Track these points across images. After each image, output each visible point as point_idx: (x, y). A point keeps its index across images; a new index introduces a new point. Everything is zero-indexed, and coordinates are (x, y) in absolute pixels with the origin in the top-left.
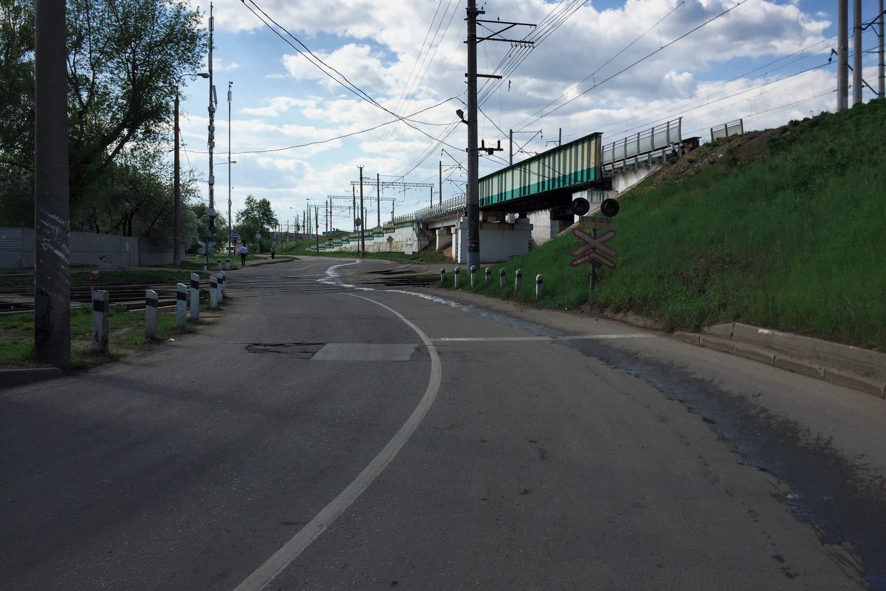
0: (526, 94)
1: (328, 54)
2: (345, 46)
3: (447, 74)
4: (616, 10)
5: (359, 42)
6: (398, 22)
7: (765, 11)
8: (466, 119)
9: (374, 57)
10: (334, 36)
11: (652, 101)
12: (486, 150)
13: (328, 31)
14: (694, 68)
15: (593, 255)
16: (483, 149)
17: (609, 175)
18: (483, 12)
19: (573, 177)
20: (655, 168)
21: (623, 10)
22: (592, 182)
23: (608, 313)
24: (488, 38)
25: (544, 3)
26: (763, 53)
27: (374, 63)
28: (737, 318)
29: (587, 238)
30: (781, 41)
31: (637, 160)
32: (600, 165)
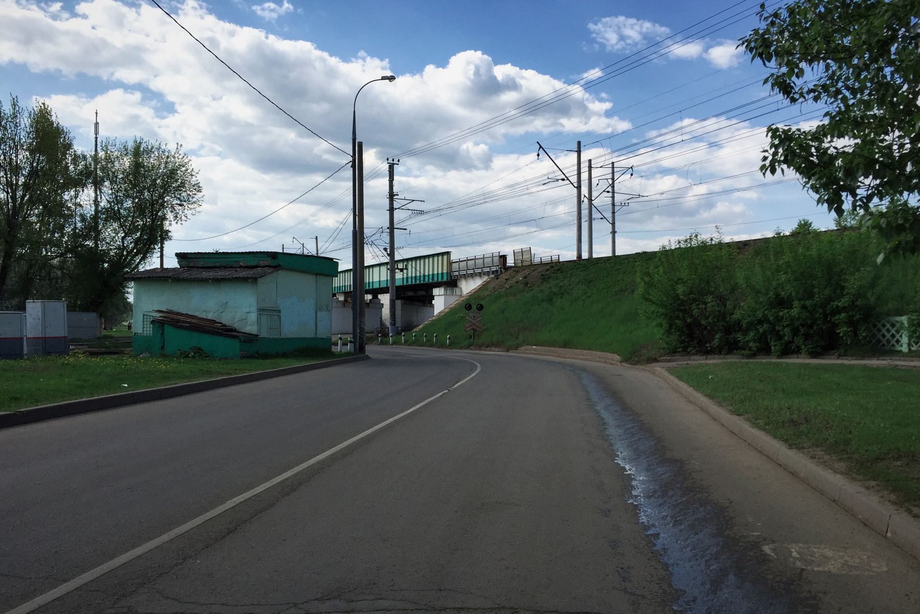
0: (321, 156)
1: (89, 99)
2: (110, 91)
3: (233, 130)
4: (414, 76)
5: (128, 88)
6: (176, 69)
7: (554, 88)
8: (389, 253)
9: (147, 106)
10: (98, 79)
11: (449, 170)
12: (399, 269)
13: (91, 72)
14: (489, 141)
15: (474, 327)
16: (398, 268)
17: (456, 278)
18: (398, 195)
19: (431, 277)
20: (485, 278)
21: (422, 77)
22: (445, 282)
23: (483, 348)
24: (399, 208)
25: (340, 62)
26: (552, 129)
27: (146, 113)
28: (528, 345)
29: (471, 320)
30: (569, 119)
31: (474, 271)
32: (450, 272)
